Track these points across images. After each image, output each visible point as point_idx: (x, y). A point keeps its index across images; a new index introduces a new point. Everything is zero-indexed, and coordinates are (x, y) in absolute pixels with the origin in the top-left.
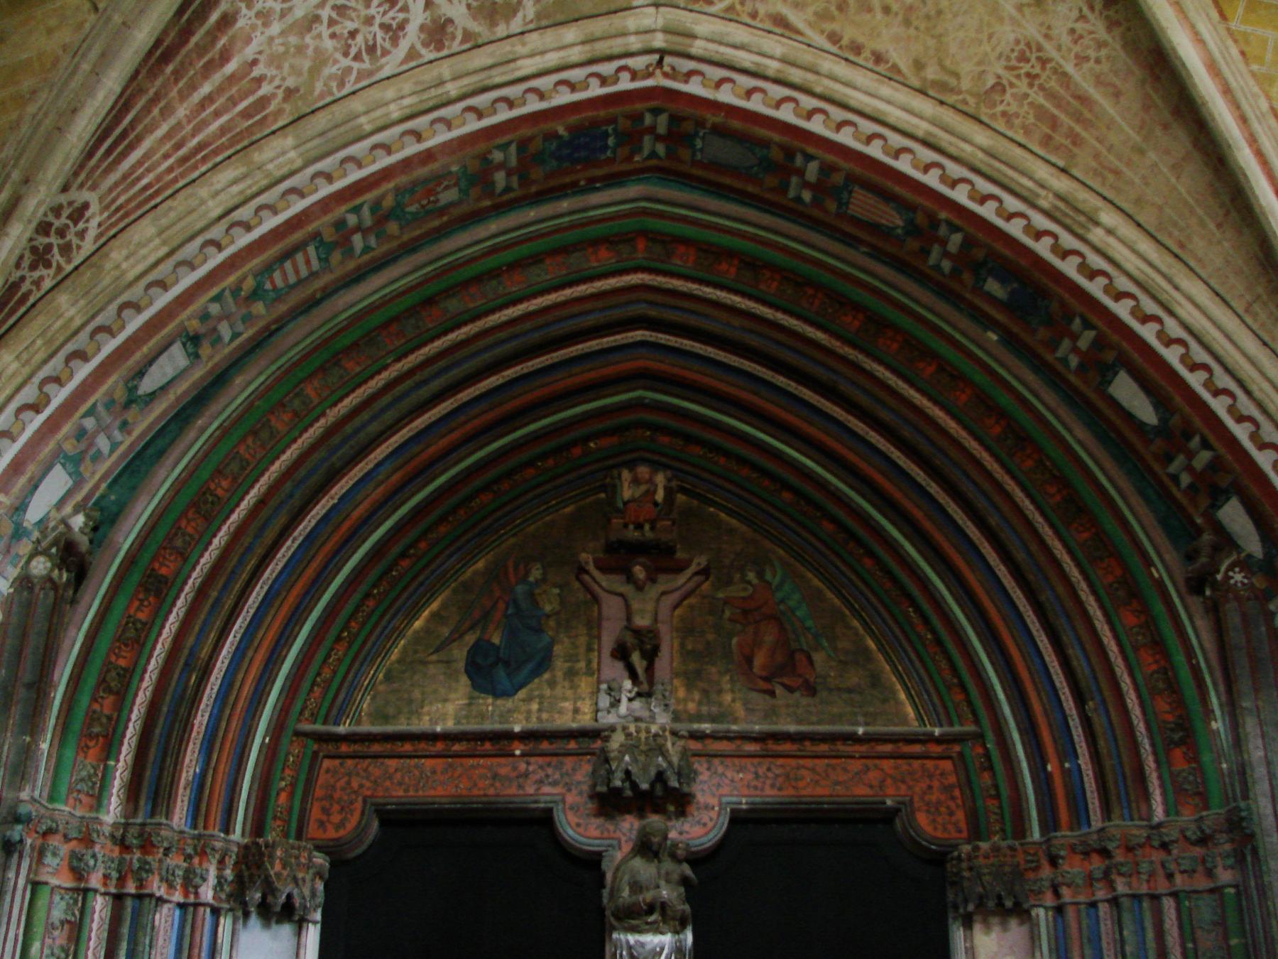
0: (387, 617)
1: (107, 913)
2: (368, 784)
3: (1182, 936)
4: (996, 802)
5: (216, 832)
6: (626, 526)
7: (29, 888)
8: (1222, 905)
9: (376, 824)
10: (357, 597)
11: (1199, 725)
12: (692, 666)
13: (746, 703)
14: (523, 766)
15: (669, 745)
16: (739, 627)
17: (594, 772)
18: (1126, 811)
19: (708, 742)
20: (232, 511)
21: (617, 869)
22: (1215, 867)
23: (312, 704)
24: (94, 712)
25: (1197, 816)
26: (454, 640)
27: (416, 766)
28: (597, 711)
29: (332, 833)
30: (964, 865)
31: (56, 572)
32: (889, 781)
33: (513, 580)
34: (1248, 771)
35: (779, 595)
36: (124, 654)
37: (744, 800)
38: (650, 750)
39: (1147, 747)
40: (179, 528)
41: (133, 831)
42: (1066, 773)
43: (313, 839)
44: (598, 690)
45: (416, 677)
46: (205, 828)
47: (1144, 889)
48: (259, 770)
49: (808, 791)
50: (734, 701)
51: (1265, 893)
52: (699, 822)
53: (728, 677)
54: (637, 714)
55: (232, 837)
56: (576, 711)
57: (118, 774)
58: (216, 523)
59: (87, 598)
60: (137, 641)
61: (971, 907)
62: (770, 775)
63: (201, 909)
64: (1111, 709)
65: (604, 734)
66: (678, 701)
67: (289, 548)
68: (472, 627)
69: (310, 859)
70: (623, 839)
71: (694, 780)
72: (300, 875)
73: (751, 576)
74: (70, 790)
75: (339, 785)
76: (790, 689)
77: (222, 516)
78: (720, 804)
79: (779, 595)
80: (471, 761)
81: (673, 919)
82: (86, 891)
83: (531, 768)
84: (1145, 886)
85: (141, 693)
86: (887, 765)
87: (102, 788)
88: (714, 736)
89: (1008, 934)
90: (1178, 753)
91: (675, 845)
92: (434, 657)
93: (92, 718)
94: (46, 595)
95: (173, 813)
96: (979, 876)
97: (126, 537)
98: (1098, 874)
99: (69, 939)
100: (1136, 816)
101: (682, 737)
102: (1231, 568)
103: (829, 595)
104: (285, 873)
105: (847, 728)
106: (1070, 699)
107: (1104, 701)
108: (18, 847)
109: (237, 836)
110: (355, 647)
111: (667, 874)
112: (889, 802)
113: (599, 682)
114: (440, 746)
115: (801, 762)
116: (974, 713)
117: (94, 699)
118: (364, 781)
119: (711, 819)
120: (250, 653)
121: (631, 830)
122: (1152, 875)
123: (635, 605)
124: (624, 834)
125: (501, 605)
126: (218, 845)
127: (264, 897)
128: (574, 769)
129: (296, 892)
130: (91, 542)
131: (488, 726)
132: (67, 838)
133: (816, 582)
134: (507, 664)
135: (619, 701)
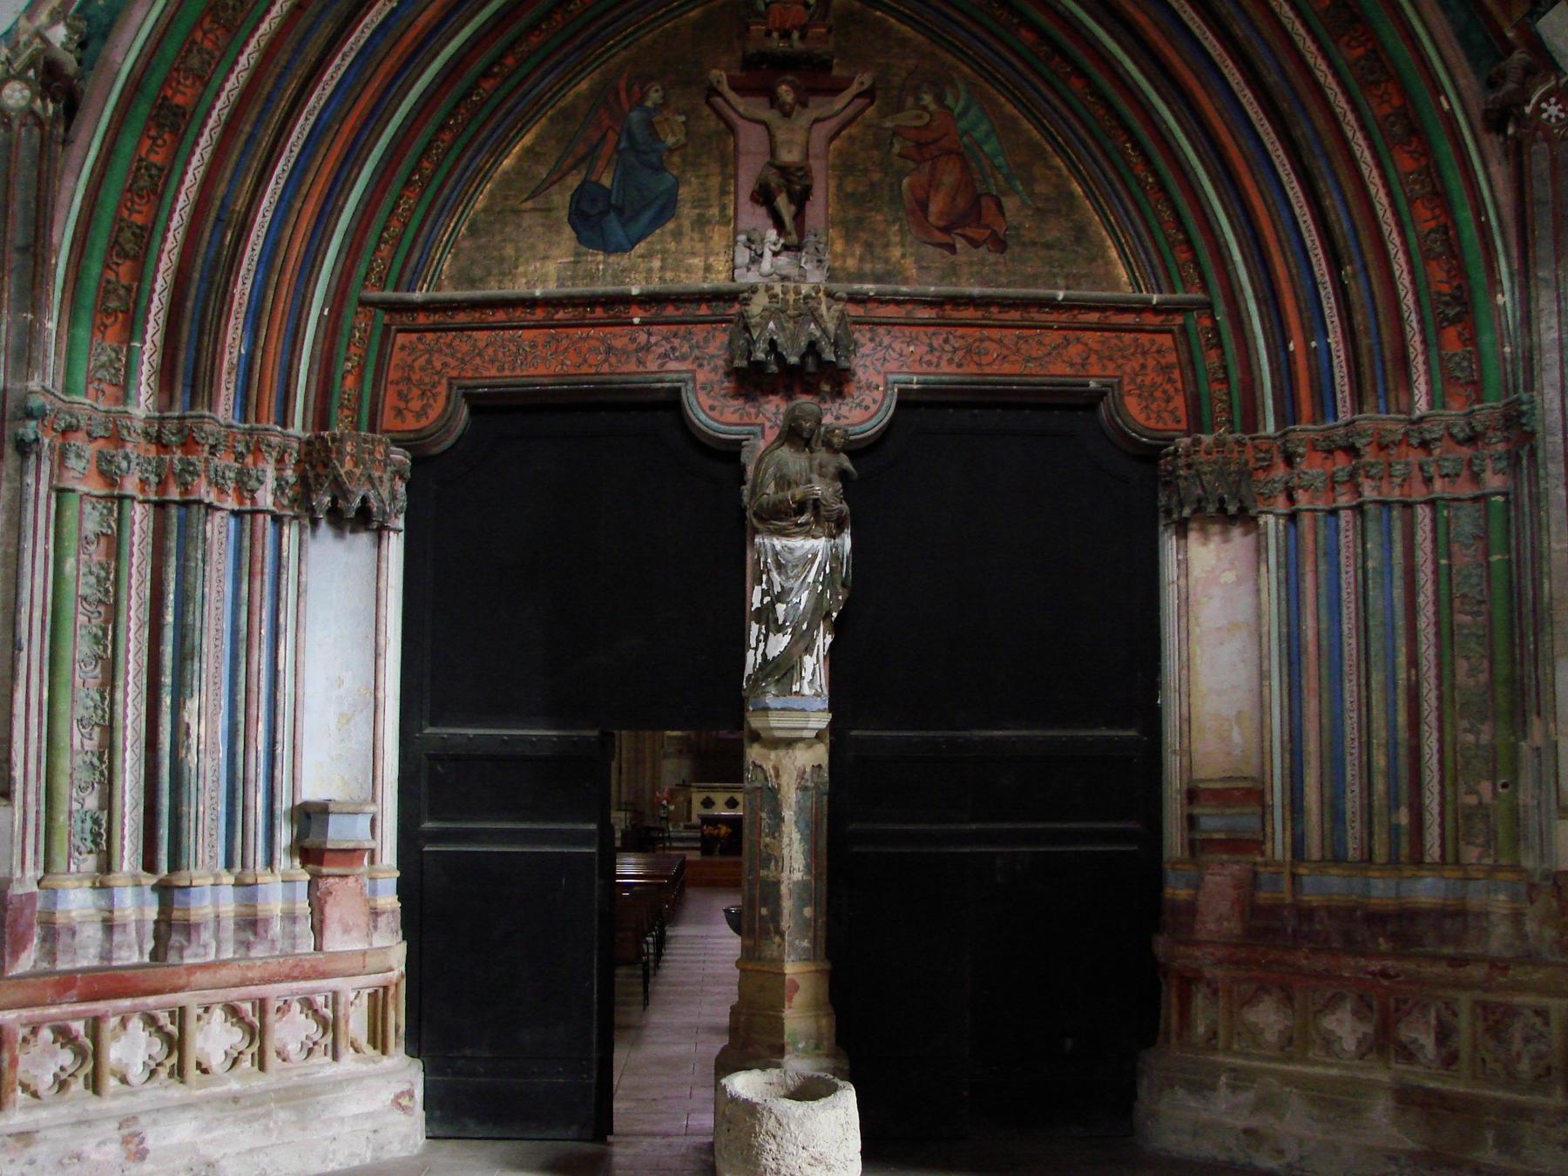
0: (469, 154)
1: (149, 525)
2: (453, 362)
3: (1435, 550)
4: (1224, 387)
5: (271, 425)
6: (768, 34)
7: (54, 495)
8: (1487, 516)
9: (465, 412)
10: (429, 130)
11: (1480, 297)
12: (852, 214)
13: (918, 261)
14: (643, 337)
15: (823, 308)
16: (912, 165)
17: (731, 342)
18: (1381, 401)
19: (870, 306)
20: (261, 19)
21: (760, 460)
22: (1484, 471)
23: (379, 266)
24: (108, 282)
25: (1467, 410)
26: (554, 183)
27: (511, 340)
28: (734, 268)
29: (412, 424)
30: (1181, 462)
31: (39, 102)
32: (1093, 358)
33: (627, 107)
34: (1536, 357)
35: (963, 125)
36: (137, 207)
37: (915, 379)
38: (800, 315)
39: (1415, 324)
40: (194, 42)
41: (171, 426)
42: (1311, 354)
43: (387, 431)
44: (735, 242)
45: (508, 230)
46: (258, 420)
47: (1396, 495)
48: (319, 348)
49: (995, 368)
50: (903, 256)
51: (1538, 501)
52: (859, 405)
53: (896, 227)
54: (784, 272)
55: (290, 431)
56: (708, 269)
57: (145, 358)
58: (243, 34)
59: (82, 138)
60: (154, 192)
61: (1186, 512)
62: (947, 348)
63: (260, 517)
64: (1374, 280)
65: (741, 296)
66: (835, 256)
67: (338, 67)
68: (575, 167)
69: (387, 456)
70: (768, 424)
71: (854, 352)
72: (377, 474)
73: (927, 99)
74: (89, 382)
75: (417, 365)
76: (974, 243)
77: (249, 25)
78: (886, 384)
79: (963, 125)
80: (579, 332)
81: (828, 520)
82: (121, 498)
83: (653, 339)
84: (1397, 491)
85: (164, 257)
86: (1091, 338)
87: (127, 376)
88: (879, 300)
89: (1227, 546)
90: (1451, 333)
91: (830, 431)
92: (529, 205)
93: (106, 290)
94: (30, 132)
95: (217, 402)
96: (1199, 474)
97: (126, 54)
98: (1342, 476)
99: (108, 555)
100: (1393, 408)
101: (839, 299)
102: (1545, 98)
103: (1026, 125)
104: (358, 472)
105: (1042, 292)
106: (1323, 262)
107: (1365, 267)
108: (34, 446)
109: (296, 429)
110: (430, 194)
111: (821, 466)
112: (1093, 384)
113: (736, 233)
114: (539, 314)
115: (986, 332)
116: (1202, 277)
117: (107, 266)
118: (449, 360)
119: (875, 402)
120: (298, 205)
121: (776, 414)
122: (1406, 479)
123: (781, 136)
124: (769, 420)
125: (612, 136)
126: (275, 440)
127: (334, 500)
128: (706, 340)
129: (372, 494)
130: (80, 62)
131: (600, 288)
132: (91, 437)
133: (1009, 109)
134: (620, 211)
135: (761, 255)
